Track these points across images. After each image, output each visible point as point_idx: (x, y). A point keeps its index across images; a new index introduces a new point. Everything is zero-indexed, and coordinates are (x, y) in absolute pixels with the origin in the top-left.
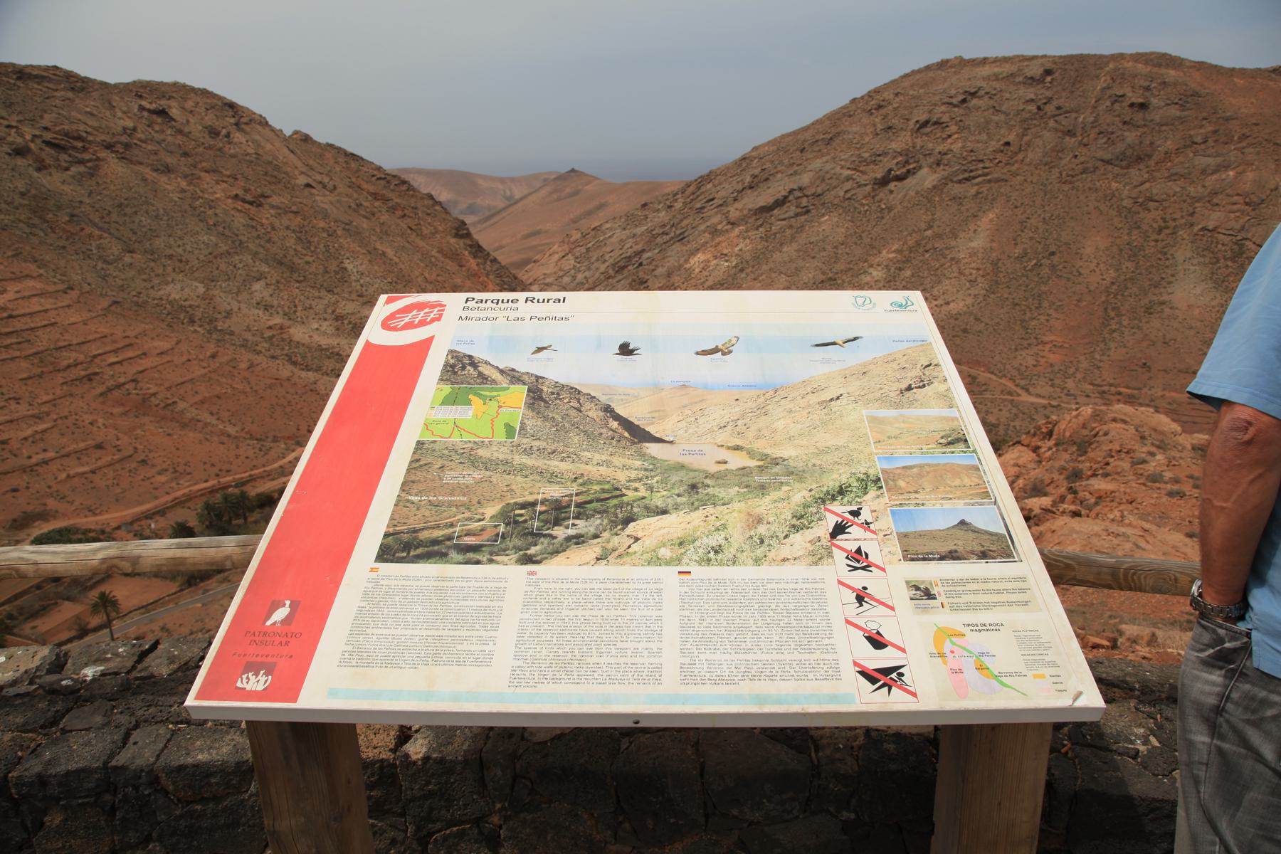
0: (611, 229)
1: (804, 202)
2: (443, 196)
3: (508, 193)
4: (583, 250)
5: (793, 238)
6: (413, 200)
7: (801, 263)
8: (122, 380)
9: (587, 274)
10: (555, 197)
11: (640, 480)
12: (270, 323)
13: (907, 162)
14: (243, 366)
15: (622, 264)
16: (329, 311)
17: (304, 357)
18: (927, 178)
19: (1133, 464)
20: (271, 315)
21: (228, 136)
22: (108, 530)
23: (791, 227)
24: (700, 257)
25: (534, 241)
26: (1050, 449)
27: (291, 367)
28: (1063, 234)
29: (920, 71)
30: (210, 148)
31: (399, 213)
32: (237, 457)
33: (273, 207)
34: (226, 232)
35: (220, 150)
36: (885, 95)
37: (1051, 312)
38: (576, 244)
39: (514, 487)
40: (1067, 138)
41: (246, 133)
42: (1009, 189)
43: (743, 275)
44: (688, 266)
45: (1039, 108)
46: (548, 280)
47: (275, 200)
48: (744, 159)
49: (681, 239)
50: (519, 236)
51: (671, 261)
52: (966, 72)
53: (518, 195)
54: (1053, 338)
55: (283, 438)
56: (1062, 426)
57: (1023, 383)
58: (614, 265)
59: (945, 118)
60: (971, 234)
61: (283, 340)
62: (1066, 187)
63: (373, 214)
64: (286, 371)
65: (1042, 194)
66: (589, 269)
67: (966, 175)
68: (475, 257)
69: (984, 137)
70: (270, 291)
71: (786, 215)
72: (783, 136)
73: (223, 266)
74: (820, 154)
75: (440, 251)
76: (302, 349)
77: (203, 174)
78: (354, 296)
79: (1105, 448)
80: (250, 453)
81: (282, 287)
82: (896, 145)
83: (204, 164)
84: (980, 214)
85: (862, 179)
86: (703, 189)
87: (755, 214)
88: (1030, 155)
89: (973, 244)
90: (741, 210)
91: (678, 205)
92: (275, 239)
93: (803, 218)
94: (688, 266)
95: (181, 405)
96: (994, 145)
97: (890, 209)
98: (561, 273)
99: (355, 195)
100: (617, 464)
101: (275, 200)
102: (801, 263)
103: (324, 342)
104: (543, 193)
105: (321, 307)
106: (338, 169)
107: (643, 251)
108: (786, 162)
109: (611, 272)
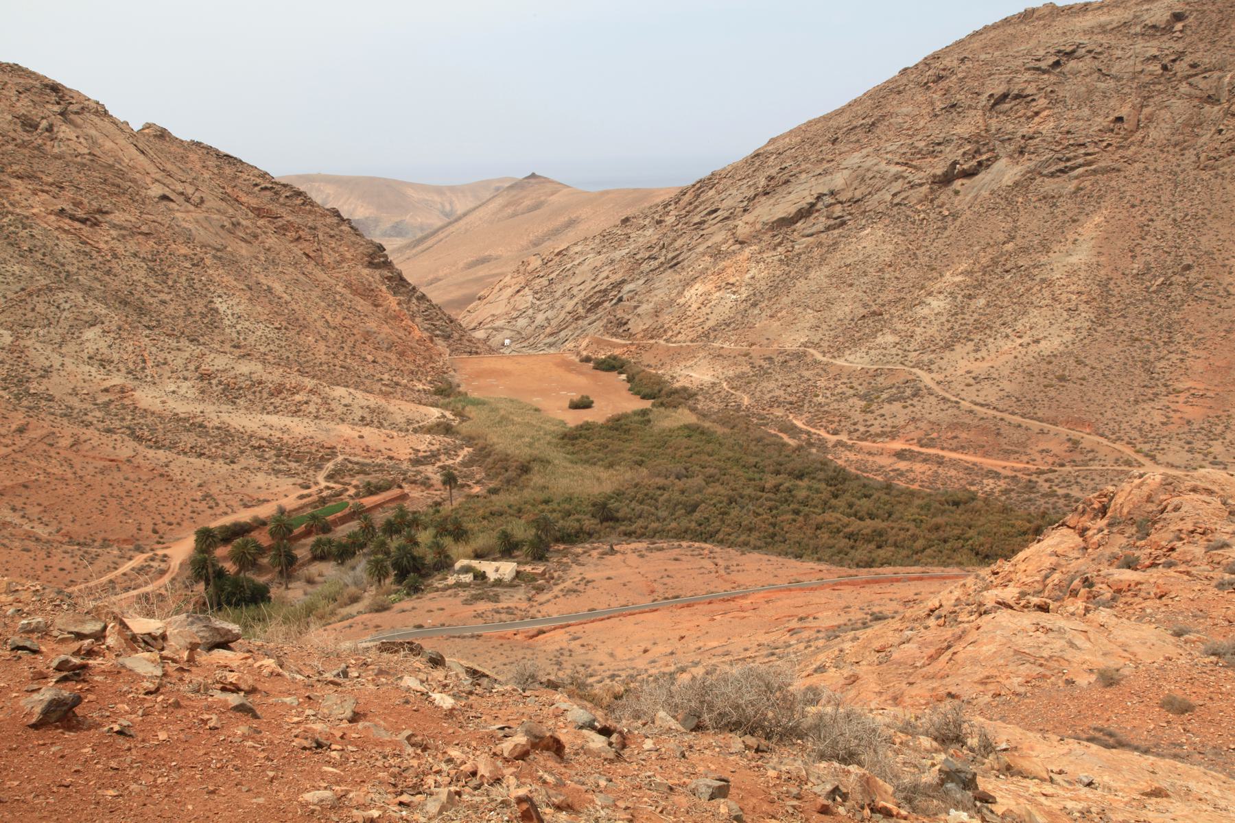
0: (582, 253)
1: (838, 210)
2: (355, 210)
3: (448, 208)
4: (544, 282)
5: (823, 260)
6: (311, 217)
7: (834, 293)
9: (550, 314)
10: (510, 211)
11: (433, 457)
12: (107, 384)
13: (978, 152)
14: (65, 442)
16: (192, 367)
17: (153, 430)
18: (1006, 172)
19: (1208, 549)
20: (109, 372)
21: (50, 129)
23: (820, 244)
24: (699, 288)
25: (482, 271)
26: (1101, 530)
27: (133, 444)
28: (1203, 240)
29: (995, 27)
30: (23, 145)
31: (292, 234)
32: (47, 568)
33: (114, 226)
34: (47, 260)
35: (39, 148)
36: (947, 62)
37: (1188, 348)
39: (214, 490)
40: (1207, 107)
41: (76, 126)
42: (1122, 181)
43: (756, 311)
44: (682, 301)
45: (1165, 68)
46: (498, 323)
47: (118, 217)
48: (757, 155)
49: (674, 264)
50: (461, 265)
51: (660, 295)
52: (1060, 24)
53: (460, 209)
54: (1189, 384)
55: (118, 541)
56: (1119, 500)
57: (1146, 448)
58: (584, 301)
59: (1031, 89)
60: (1070, 246)
61: (124, 407)
62: (1205, 175)
63: (256, 237)
64: (127, 448)
65: (1170, 185)
66: (552, 307)
67: (1062, 165)
68: (395, 294)
69: (1086, 112)
70: (109, 340)
71: (814, 230)
72: (810, 124)
73: (41, 307)
75: (348, 285)
76: (150, 420)
77: (13, 181)
78: (227, 347)
79: (1173, 527)
80: (67, 563)
81: (125, 335)
82: (964, 129)
83: (15, 168)
84: (1082, 218)
85: (917, 177)
86: (703, 197)
87: (772, 229)
88: (1153, 133)
89: (1073, 259)
90: (753, 224)
91: (670, 220)
92: (117, 270)
94: (682, 301)
96: (1100, 122)
97: (955, 216)
98: (515, 314)
99: (231, 211)
100: (400, 419)
101: (118, 217)
102: (834, 293)
103: (182, 409)
104: (493, 206)
105: (180, 362)
106: (207, 176)
107: (623, 282)
108: (813, 157)
109: (581, 311)
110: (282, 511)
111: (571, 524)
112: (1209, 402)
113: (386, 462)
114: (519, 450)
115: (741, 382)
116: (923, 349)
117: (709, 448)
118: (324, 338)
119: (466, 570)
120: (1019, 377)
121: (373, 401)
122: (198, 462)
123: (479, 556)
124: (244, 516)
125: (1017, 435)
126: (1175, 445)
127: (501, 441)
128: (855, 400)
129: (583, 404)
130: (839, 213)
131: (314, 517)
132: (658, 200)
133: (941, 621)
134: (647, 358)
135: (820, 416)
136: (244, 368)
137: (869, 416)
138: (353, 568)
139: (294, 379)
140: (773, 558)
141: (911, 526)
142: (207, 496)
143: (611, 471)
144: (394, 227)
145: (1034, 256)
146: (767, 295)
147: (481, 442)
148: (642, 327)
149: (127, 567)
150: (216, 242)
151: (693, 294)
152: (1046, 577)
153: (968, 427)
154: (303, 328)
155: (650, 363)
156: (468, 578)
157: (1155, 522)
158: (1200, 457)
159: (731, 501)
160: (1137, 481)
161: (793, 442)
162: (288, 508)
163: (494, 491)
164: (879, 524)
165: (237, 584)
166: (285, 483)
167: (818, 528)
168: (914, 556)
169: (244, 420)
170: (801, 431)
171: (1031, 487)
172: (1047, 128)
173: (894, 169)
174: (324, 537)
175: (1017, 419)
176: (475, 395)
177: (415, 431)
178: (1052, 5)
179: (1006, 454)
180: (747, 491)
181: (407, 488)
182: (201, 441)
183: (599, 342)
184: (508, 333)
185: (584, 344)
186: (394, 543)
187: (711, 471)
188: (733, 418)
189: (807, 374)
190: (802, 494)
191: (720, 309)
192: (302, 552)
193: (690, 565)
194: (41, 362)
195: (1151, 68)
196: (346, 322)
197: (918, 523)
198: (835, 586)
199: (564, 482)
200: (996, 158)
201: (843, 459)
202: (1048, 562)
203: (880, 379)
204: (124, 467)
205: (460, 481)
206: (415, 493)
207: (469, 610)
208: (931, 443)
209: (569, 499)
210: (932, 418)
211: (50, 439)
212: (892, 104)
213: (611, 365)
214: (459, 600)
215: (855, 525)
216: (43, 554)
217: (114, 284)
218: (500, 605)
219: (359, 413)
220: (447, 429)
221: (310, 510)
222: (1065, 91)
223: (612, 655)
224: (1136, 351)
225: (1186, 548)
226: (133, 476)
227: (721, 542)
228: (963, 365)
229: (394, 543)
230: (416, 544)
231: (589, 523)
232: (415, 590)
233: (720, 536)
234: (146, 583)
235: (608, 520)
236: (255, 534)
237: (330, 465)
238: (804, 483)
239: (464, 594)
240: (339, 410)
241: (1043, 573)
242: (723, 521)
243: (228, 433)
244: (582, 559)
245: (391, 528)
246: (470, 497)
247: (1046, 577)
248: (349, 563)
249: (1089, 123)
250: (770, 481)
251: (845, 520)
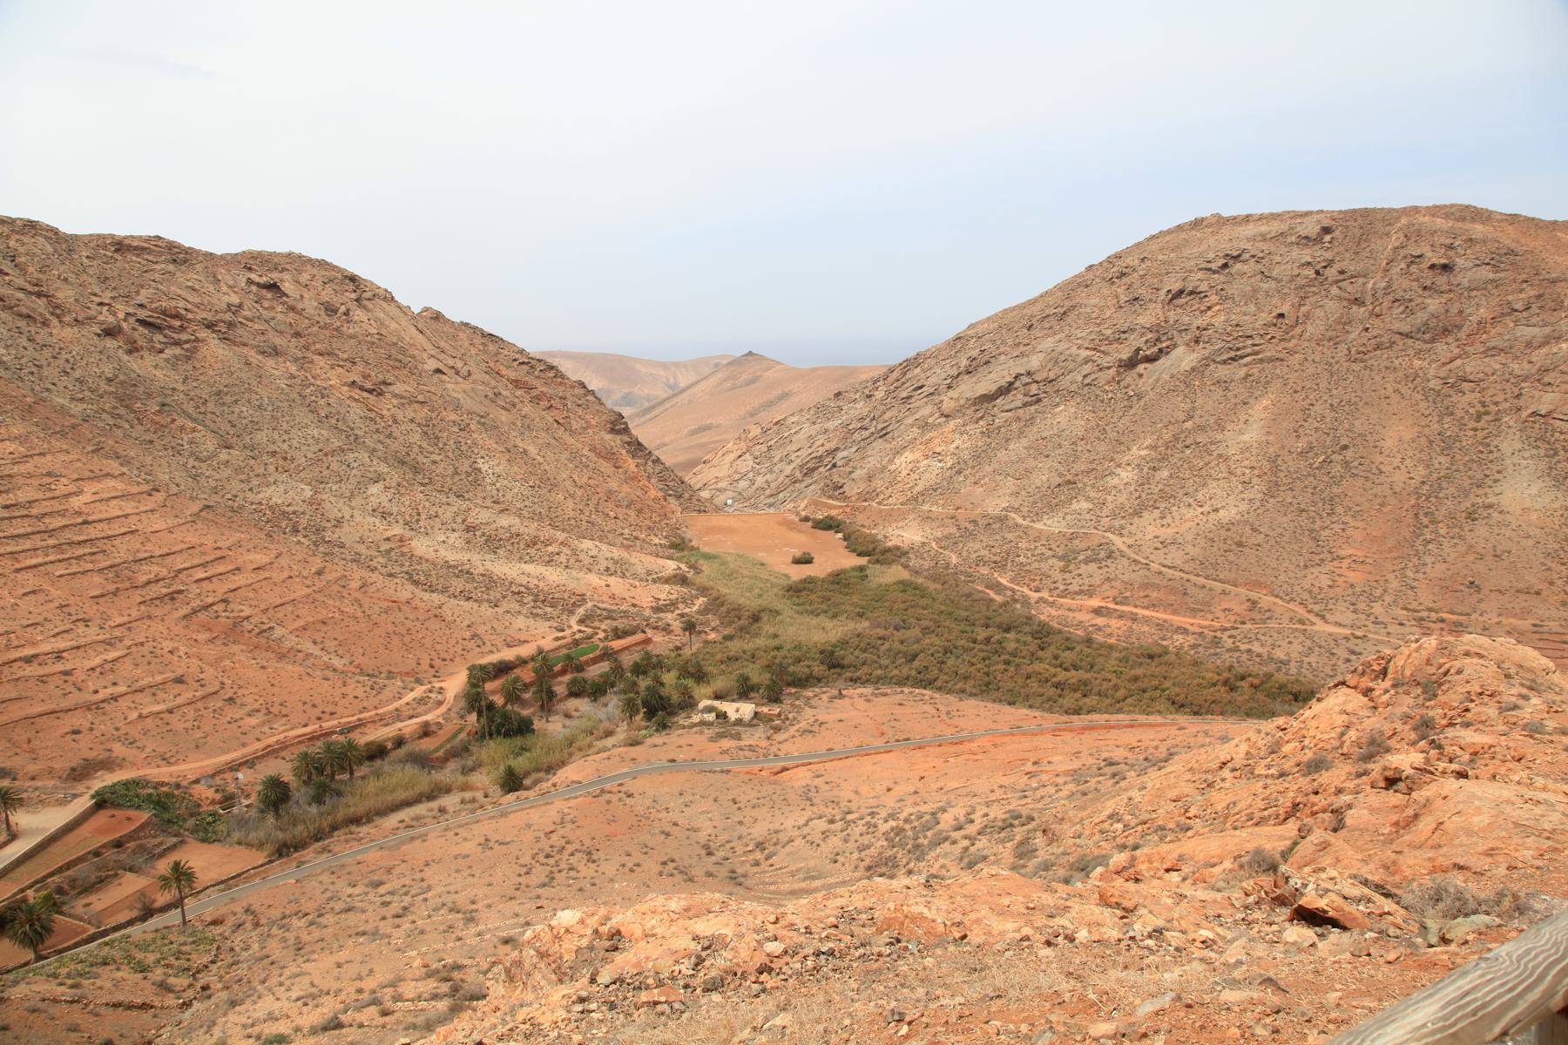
1: (1034, 389)
4: (764, 448)
5: (1021, 433)
7: (1031, 463)
8: (210, 600)
10: (729, 384)
11: (673, 605)
12: (388, 534)
13: (1158, 340)
14: (354, 585)
15: (810, 465)
17: (428, 576)
18: (1183, 358)
19: (1501, 710)
20: (390, 524)
21: (347, 313)
22: (184, 783)
23: (1019, 419)
24: (908, 456)
25: (704, 438)
27: (411, 587)
28: (1357, 423)
29: (1169, 232)
30: (325, 327)
31: (544, 404)
33: (396, 396)
34: (340, 425)
35: (336, 329)
36: (1129, 261)
37: (1348, 519)
39: (481, 630)
42: (1286, 370)
44: (892, 467)
45: (1317, 273)
46: (721, 485)
47: (399, 388)
49: (884, 434)
51: (872, 462)
52: (1226, 232)
54: (1351, 551)
55: (400, 673)
56: (1399, 662)
57: (1316, 608)
59: (1203, 287)
61: (403, 554)
62: (1356, 367)
63: (514, 405)
64: (406, 592)
66: (771, 471)
67: (1232, 354)
73: (334, 466)
75: (593, 449)
76: (425, 566)
77: (316, 358)
78: (488, 503)
80: (360, 692)
81: (403, 490)
82: (1147, 319)
85: (1105, 361)
88: (1310, 329)
89: (1246, 437)
91: (880, 394)
95: (279, 632)
96: (1265, 317)
97: (1139, 397)
98: (736, 477)
99: (493, 383)
100: (640, 570)
101: (399, 388)
102: (1031, 463)
103: (452, 557)
104: (714, 380)
105: (449, 515)
107: (837, 449)
109: (798, 475)
110: (540, 651)
111: (800, 670)
112: (1369, 568)
113: (631, 609)
114: (750, 602)
115: (948, 542)
116: (1114, 516)
117: (924, 601)
118: (572, 496)
119: (710, 709)
120: (1202, 542)
121: (617, 553)
122: (467, 605)
123: (718, 697)
124: (508, 655)
125: (1202, 595)
126: (1341, 606)
127: (731, 592)
128: (1055, 560)
129: (805, 560)
130: (1034, 391)
131: (569, 657)
132: (865, 377)
133: (1237, 774)
134: (861, 519)
135: (1022, 574)
136: (504, 521)
137: (1067, 576)
138: (606, 705)
139: (547, 532)
140: (989, 705)
141: (1113, 677)
142: (474, 636)
143: (835, 622)
144: (624, 398)
145: (1211, 433)
146: (970, 463)
147: (714, 593)
148: (856, 490)
149: (410, 697)
150: (481, 410)
151: (903, 462)
152: (1343, 734)
153: (1157, 587)
154: (554, 486)
155: (863, 522)
156: (711, 717)
157: (1440, 685)
158: (1363, 617)
159: (946, 651)
160: (1414, 646)
161: (999, 599)
162: (547, 648)
163: (728, 638)
164: (1082, 674)
165: (506, 717)
166: (542, 627)
167: (1029, 677)
168: (1117, 705)
169: (505, 568)
170: (1006, 588)
171: (1216, 642)
172: (1219, 321)
173: (1085, 353)
174: (579, 676)
175: (1201, 581)
176: (705, 549)
177: (654, 581)
178: (1219, 216)
179: (1193, 612)
180: (962, 642)
181: (650, 633)
182: (469, 586)
183: (816, 504)
184: (730, 494)
185: (803, 505)
186: (644, 683)
187: (925, 623)
188: (942, 575)
189: (1009, 536)
190: (1011, 646)
191: (927, 475)
192: (560, 689)
193: (915, 710)
194: (334, 513)
195: (1306, 272)
196: (591, 482)
197: (1119, 674)
198: (1055, 732)
199: (791, 630)
200: (1175, 346)
201: (1045, 614)
202: (1340, 720)
203: (1076, 542)
204: (404, 608)
205: (698, 628)
206: (658, 638)
207: (715, 747)
208: (1125, 601)
209: (798, 647)
210: (1125, 578)
211: (343, 581)
212: (1081, 296)
213: (828, 525)
214: (704, 738)
215: (1062, 676)
216: (339, 683)
217: (394, 446)
218: (742, 743)
219: (604, 564)
220: (683, 580)
221: (565, 651)
222: (1232, 290)
223: (856, 792)
224: (1303, 521)
225: (1480, 709)
226: (412, 616)
227: (940, 689)
228: (1151, 531)
229: (644, 683)
230: (662, 684)
231: (818, 669)
232: (663, 726)
233: (939, 683)
234: (426, 713)
235: (835, 666)
236: (517, 671)
237: (581, 611)
238: (1011, 636)
239: (709, 732)
240: (587, 561)
241: (1338, 730)
242: (940, 670)
243: (491, 580)
244: (814, 702)
245: (638, 669)
246: (706, 642)
247: (1343, 734)
248: (602, 700)
249: (1256, 318)
250: (982, 634)
251: (1053, 670)
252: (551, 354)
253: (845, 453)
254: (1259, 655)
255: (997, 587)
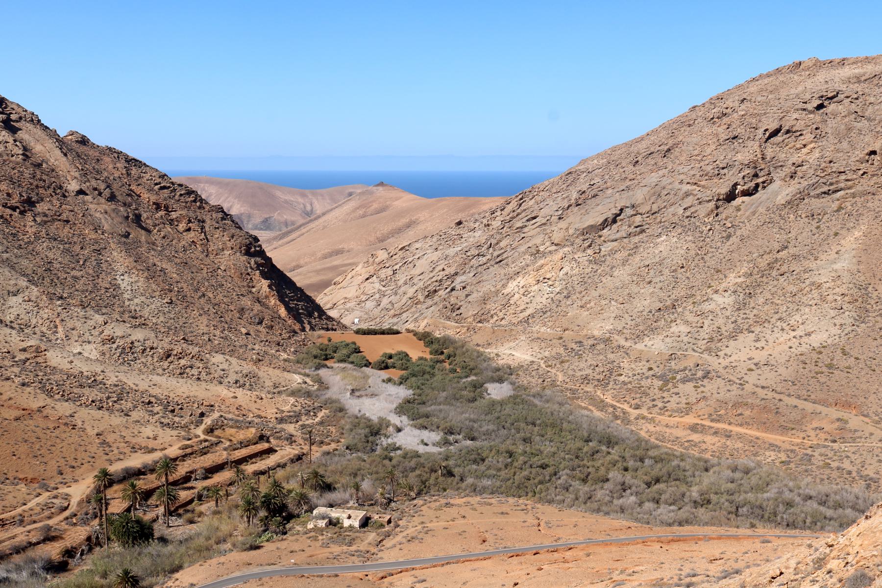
2: (235, 209)
3: (309, 208)
4: (389, 272)
5: (625, 262)
10: (361, 212)
12: (24, 345)
13: (756, 175)
16: (96, 332)
18: (780, 191)
24: (521, 281)
25: (337, 261)
29: (768, 75)
36: (729, 103)
38: (382, 265)
39: (110, 438)
44: (506, 291)
50: (319, 255)
52: (822, 76)
66: (396, 294)
71: (618, 235)
74: (657, 168)
82: (744, 156)
89: (838, 266)
91: (496, 224)
93: (636, 239)
98: (364, 298)
102: (634, 289)
107: (456, 274)
109: (421, 297)
124: (136, 461)
137: (665, 394)
175: (793, 401)
179: (784, 429)
201: (645, 430)
219: (232, 378)
252: (197, 181)
253: (463, 278)
254: (850, 473)
255: (602, 405)
